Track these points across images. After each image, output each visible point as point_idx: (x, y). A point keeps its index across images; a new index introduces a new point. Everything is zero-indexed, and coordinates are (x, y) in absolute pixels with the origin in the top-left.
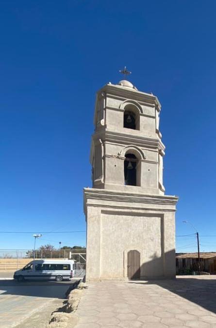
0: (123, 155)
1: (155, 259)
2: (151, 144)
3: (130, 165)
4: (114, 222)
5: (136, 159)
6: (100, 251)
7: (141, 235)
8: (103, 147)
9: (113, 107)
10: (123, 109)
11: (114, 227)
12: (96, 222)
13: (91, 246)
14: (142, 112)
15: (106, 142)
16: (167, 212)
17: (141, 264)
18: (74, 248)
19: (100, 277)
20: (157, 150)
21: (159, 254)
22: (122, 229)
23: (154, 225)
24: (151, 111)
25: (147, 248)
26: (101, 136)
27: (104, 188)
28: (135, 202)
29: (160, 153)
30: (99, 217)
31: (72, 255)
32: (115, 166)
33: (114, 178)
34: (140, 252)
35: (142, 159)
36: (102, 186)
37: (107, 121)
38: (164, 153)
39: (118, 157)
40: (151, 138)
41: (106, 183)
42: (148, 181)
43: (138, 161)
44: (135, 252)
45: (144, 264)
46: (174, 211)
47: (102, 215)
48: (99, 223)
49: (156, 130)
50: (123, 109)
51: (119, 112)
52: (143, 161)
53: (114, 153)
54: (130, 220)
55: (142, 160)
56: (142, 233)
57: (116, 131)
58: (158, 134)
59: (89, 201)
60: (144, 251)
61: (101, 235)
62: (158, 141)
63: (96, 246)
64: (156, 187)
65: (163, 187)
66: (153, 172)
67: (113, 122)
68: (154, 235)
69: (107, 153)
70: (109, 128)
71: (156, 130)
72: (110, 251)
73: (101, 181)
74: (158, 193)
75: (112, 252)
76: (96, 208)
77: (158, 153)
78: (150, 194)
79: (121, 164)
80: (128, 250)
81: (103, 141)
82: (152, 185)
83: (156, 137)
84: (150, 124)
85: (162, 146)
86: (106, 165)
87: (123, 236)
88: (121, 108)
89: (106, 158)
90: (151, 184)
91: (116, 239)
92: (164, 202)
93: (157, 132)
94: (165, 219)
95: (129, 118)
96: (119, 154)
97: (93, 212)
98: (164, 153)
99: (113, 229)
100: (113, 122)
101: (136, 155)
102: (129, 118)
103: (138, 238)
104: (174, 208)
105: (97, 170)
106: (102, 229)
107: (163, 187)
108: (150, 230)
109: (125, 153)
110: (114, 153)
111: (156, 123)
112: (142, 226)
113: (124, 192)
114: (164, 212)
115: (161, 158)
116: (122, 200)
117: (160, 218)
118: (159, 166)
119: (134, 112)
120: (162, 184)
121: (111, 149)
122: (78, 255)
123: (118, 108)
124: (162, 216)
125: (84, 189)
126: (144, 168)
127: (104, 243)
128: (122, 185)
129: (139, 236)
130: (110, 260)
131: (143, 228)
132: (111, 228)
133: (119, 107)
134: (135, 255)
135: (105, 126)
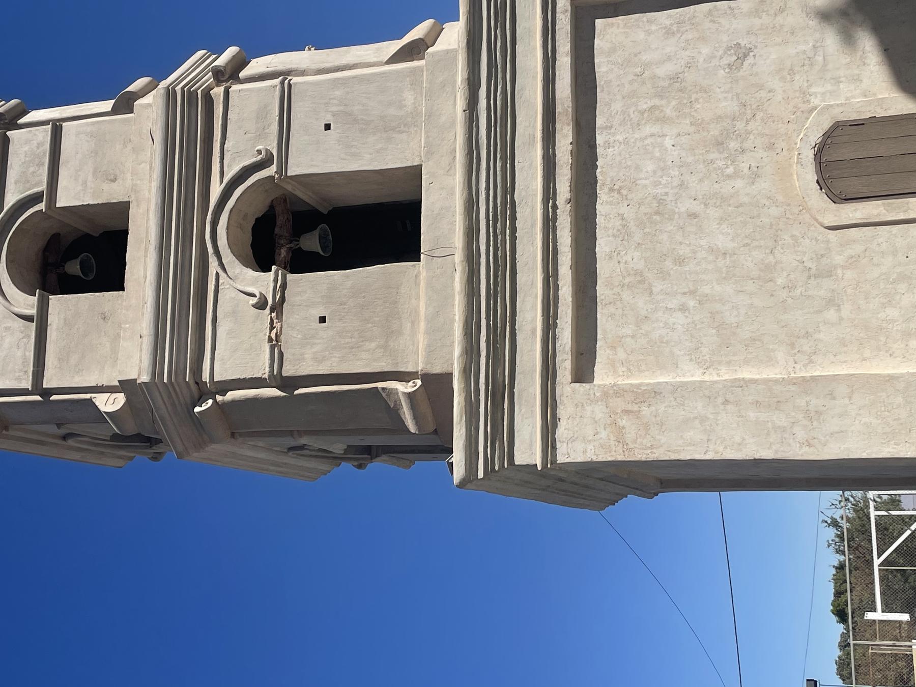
0: (263, 282)
2: (192, 132)
3: (311, 243)
4: (642, 304)
5: (279, 209)
6: (835, 377)
7: (715, 131)
8: (231, 395)
9: (31, 355)
10: (34, 300)
11: (673, 303)
12: (646, 411)
13: (801, 434)
14: (36, 198)
15: (206, 377)
18: (841, 615)
19: (420, 369)
20: (218, 92)
22: (684, 251)
23: (646, 57)
24: (26, 145)
25: (800, 80)
26: (171, 415)
27: (450, 376)
28: (509, 189)
29: (230, 74)
30: (619, 392)
31: (887, 608)
32: (323, 320)
33: (398, 324)
34: (827, 125)
35: (271, 171)
36: (436, 387)
37: (104, 381)
38: (232, 51)
39: (278, 308)
40: (159, 136)
41: (420, 367)
42: (390, 128)
43: (286, 199)
44: (831, 155)
47: (602, 376)
48: (655, 392)
49: (115, 111)
50: (34, 300)
51: (54, 319)
53: (267, 330)
54: (624, 210)
55: (279, 171)
56: (699, 125)
57: (145, 325)
58: (136, 96)
59: (528, 451)
60: (815, 101)
61: (726, 375)
62: (170, 94)
63: (801, 402)
64: (420, 69)
65: (417, 32)
66: (350, 106)
67: (107, 346)
68: (706, 50)
69: (262, 369)
70: (137, 368)
71: (115, 111)
72: (831, 315)
73: (410, 396)
74: (449, 55)
75: (832, 302)
76: (561, 412)
77: (235, 88)
78: (461, 103)
79: (311, 289)
80: (818, 199)
81: (203, 392)
82: (409, 98)
83: (150, 106)
84: (103, 153)
85: (194, 68)
86: (323, 369)
87: (730, 245)
88: (33, 311)
89: (289, 370)
90: (401, 106)
91: (750, 286)
93: (125, 105)
95: (74, 268)
96: (261, 305)
97: (589, 431)
98: (232, 51)
99: (683, 308)
100: (107, 346)
101: (258, 208)
102: (74, 268)
103: (733, 145)
105: (359, 427)
106: (693, 375)
107: (417, 32)
108: (675, 78)
109: (250, 273)
110: (267, 330)
111: (86, 123)
112: (655, 129)
113: (459, 257)
115: (257, 65)
116: (505, 267)
117: (599, 23)
118: (303, 73)
119: (41, 243)
120: (394, 46)
121: (237, 351)
122: (878, 518)
123: (33, 326)
125: (463, 484)
126: (318, 156)
127: (780, 355)
128: (423, 274)
129: (719, 144)
130: (892, 313)
131: (664, 120)
132: (679, 319)
133: (29, 319)
134: (845, 153)
135: (126, 386)
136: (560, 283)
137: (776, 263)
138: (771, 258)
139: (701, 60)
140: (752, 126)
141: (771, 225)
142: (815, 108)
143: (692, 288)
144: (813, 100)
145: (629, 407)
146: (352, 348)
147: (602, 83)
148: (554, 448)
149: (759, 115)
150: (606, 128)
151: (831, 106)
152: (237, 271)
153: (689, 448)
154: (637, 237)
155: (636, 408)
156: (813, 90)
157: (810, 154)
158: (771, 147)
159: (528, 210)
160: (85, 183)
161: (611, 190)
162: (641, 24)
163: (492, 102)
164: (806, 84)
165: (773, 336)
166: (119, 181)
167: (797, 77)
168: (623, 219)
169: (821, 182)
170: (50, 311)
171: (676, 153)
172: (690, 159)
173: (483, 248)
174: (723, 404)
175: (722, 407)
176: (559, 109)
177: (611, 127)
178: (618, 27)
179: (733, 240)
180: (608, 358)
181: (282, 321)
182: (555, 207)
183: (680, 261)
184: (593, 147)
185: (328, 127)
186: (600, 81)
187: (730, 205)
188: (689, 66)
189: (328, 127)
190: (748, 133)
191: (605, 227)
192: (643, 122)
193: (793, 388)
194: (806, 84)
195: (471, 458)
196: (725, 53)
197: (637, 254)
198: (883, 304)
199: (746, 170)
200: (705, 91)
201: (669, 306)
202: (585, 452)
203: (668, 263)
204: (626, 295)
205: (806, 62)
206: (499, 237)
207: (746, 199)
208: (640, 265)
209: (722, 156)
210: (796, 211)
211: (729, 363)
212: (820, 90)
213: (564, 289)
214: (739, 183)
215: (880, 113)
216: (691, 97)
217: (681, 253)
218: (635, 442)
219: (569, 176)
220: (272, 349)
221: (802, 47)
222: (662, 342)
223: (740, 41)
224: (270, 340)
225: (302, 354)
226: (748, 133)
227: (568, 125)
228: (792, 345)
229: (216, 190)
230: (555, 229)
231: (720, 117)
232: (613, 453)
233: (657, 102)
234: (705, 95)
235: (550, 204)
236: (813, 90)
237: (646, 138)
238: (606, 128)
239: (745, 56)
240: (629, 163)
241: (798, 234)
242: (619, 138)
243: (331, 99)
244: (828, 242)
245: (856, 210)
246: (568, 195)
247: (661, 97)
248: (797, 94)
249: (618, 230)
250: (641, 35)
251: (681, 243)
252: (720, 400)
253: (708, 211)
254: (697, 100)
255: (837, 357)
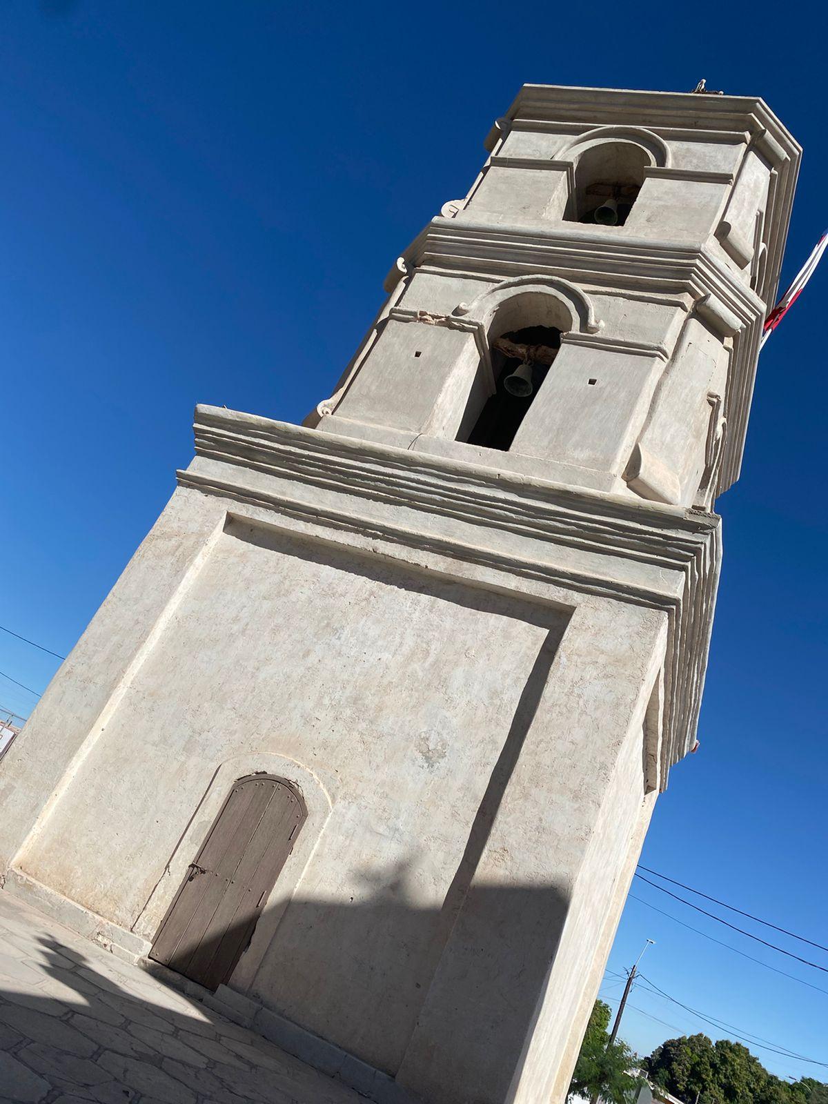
1: (388, 901)
7: (370, 700)
16: (602, 602)
17: (277, 894)
21: (432, 886)
28: (413, 503)
32: (418, 354)
34: (310, 804)
45: (290, 906)
46: (658, 602)
52: (575, 341)
54: (350, 598)
60: (341, 804)
76: (212, 498)
80: (249, 766)
90: (575, 447)
92: (594, 534)
94: (572, 639)
99: (236, 620)
104: (673, 585)
108: (444, 683)
112: (405, 650)
114: (575, 598)
117: (545, 632)
118: (667, 371)
124: (555, 620)
129: (355, 700)
131: (409, 659)
136: (309, 525)
137: (223, 708)
138: (229, 706)
139: (448, 714)
140: (356, 735)
141: (256, 717)
142: (333, 802)
143: (247, 632)
144: (343, 802)
145: (181, 549)
146: (381, 373)
147: (478, 616)
148: (189, 486)
149: (360, 748)
150: (432, 607)
151: (325, 818)
152: (498, 297)
153: (125, 583)
154: (318, 602)
155: (177, 554)
156: (354, 807)
157: (292, 778)
158: (325, 745)
159: (387, 515)
160: (659, 199)
161: (372, 593)
162: (520, 671)
163: (500, 504)
164: (363, 803)
165: (169, 682)
166: (647, 224)
167: (376, 799)
168: (341, 595)
169: (263, 776)
170: (552, 171)
171: (371, 660)
172: (358, 669)
173: (367, 466)
174: (137, 620)
175: (136, 618)
176: (466, 565)
177: (431, 611)
178: (529, 648)
179: (265, 680)
180: (236, 549)
181: (436, 325)
182: (375, 537)
183: (276, 630)
184: (420, 590)
185: (592, 382)
186: (481, 615)
187: (296, 688)
188: (449, 700)
189: (592, 382)
190: (350, 730)
191: (343, 578)
192: (419, 641)
193: (113, 677)
194: (363, 803)
195: (209, 420)
196: (442, 740)
197: (303, 597)
198: (134, 783)
199: (317, 715)
200: (414, 706)
201: (246, 608)
202: (173, 508)
203: (279, 620)
204: (276, 578)
205: (386, 814)
206: (373, 483)
207: (291, 705)
208: (293, 598)
209: (343, 699)
210: (254, 744)
211: (172, 639)
212: (349, 815)
213: (303, 527)
214: (310, 704)
215: (291, 860)
216: (416, 691)
217: (282, 634)
218: (155, 546)
219: (397, 557)
220: (414, 314)
221: (403, 817)
222: (221, 594)
223: (446, 759)
224: (423, 314)
225: (398, 337)
226: (350, 730)
227: (445, 569)
228: (151, 695)
229: (579, 287)
230: (357, 532)
231: (381, 710)
232: (158, 527)
233: (431, 660)
234: (411, 704)
235: (379, 533)
236: (354, 807)
237: (402, 638)
238: (432, 607)
239: (428, 759)
240: (386, 616)
241: (233, 737)
242: (416, 615)
243: (620, 388)
244: (212, 760)
245: (219, 795)
246: (380, 551)
247: (433, 665)
248: (358, 792)
249: (334, 588)
250: (506, 666)
251: (290, 636)
252: (141, 618)
253: (302, 668)
254: (411, 696)
255: (121, 726)
